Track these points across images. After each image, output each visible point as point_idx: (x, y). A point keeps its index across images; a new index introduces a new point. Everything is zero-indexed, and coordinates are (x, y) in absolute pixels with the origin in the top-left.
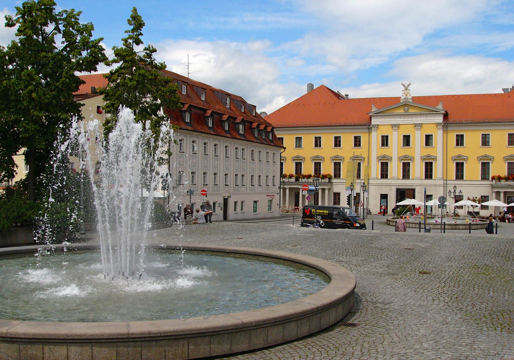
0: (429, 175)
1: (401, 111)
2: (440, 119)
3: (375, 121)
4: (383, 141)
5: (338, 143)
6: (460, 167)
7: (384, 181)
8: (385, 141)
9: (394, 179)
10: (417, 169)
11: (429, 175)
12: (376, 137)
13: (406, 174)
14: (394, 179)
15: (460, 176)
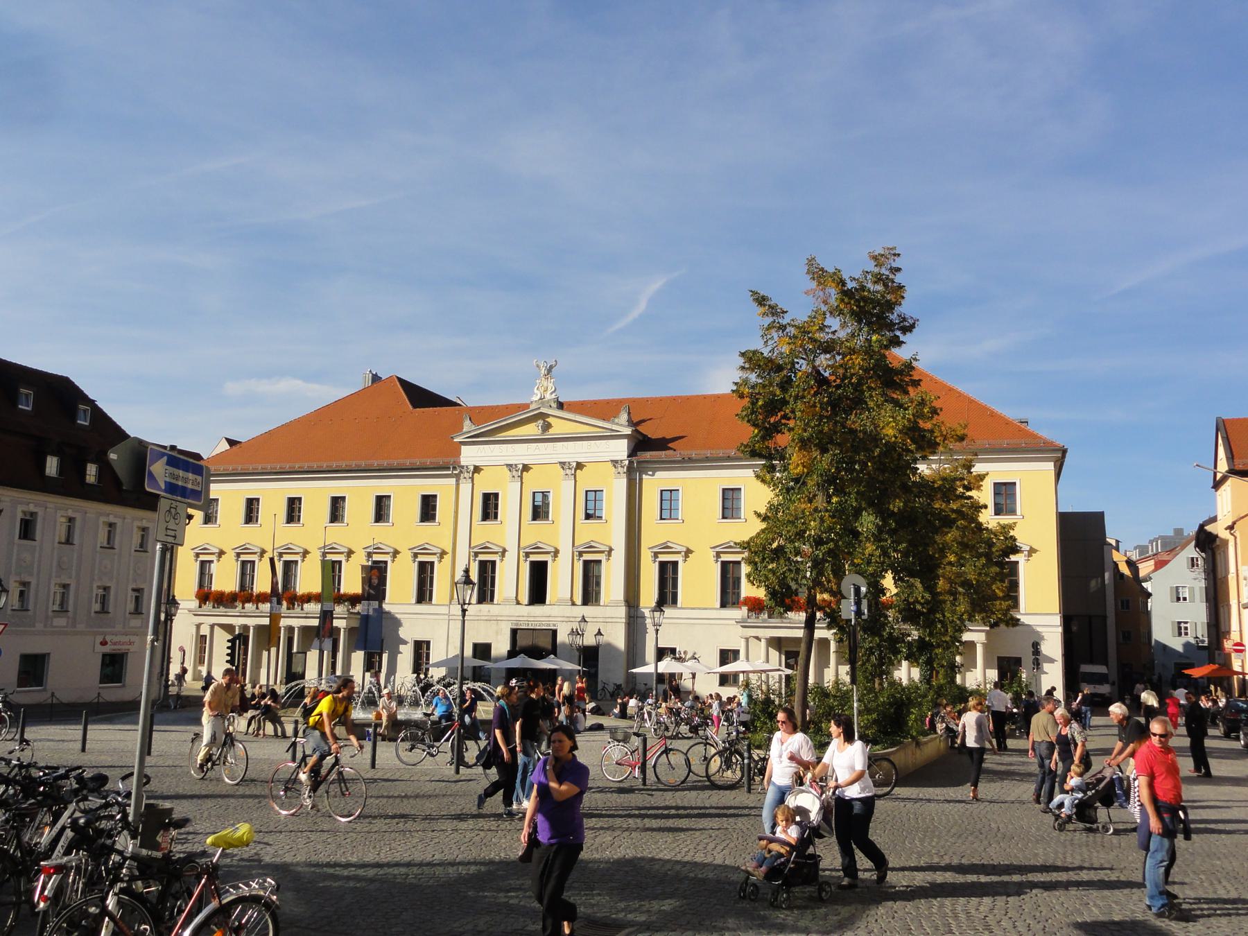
0: (590, 594)
1: (532, 430)
2: (620, 449)
3: (470, 455)
4: (1012, 496)
5: (492, 511)
6: (668, 573)
7: (423, 608)
8: (490, 507)
9: (560, 602)
10: (562, 580)
11: (590, 594)
12: (468, 498)
13: (538, 594)
14: (560, 602)
15: (667, 596)
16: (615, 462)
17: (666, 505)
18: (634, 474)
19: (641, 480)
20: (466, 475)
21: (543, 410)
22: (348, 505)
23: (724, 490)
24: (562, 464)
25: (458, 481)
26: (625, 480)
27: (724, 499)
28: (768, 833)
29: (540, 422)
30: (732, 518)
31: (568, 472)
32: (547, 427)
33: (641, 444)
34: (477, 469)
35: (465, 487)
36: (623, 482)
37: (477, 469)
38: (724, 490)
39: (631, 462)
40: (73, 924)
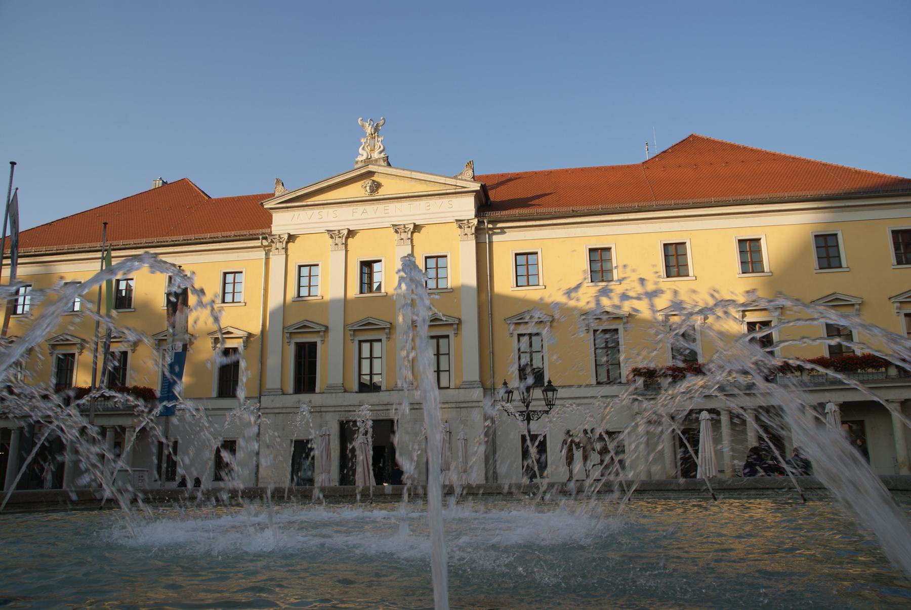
1: (358, 190)
2: (466, 207)
16: (460, 223)
17: (673, 261)
18: (482, 237)
19: (491, 243)
20: (279, 245)
21: (371, 168)
22: (616, 258)
23: (665, 245)
24: (396, 228)
25: (267, 254)
26: (474, 242)
27: (666, 256)
28: (22, 251)
29: (368, 182)
30: (679, 275)
31: (404, 236)
32: (376, 186)
33: (486, 204)
34: (291, 238)
35: (277, 260)
36: (472, 244)
37: (291, 238)
38: (665, 245)
39: (480, 222)
40: (4, 413)
